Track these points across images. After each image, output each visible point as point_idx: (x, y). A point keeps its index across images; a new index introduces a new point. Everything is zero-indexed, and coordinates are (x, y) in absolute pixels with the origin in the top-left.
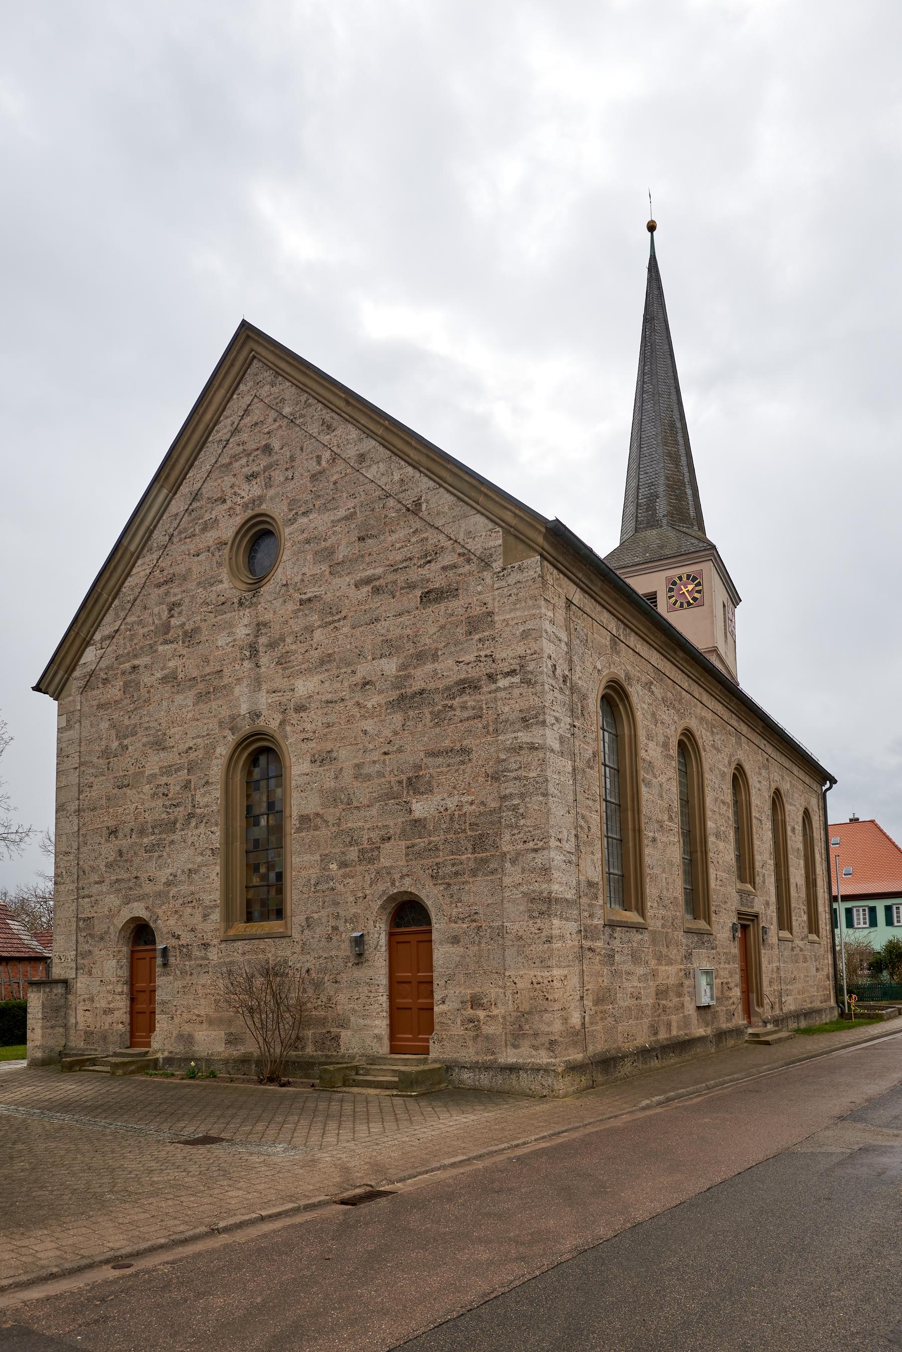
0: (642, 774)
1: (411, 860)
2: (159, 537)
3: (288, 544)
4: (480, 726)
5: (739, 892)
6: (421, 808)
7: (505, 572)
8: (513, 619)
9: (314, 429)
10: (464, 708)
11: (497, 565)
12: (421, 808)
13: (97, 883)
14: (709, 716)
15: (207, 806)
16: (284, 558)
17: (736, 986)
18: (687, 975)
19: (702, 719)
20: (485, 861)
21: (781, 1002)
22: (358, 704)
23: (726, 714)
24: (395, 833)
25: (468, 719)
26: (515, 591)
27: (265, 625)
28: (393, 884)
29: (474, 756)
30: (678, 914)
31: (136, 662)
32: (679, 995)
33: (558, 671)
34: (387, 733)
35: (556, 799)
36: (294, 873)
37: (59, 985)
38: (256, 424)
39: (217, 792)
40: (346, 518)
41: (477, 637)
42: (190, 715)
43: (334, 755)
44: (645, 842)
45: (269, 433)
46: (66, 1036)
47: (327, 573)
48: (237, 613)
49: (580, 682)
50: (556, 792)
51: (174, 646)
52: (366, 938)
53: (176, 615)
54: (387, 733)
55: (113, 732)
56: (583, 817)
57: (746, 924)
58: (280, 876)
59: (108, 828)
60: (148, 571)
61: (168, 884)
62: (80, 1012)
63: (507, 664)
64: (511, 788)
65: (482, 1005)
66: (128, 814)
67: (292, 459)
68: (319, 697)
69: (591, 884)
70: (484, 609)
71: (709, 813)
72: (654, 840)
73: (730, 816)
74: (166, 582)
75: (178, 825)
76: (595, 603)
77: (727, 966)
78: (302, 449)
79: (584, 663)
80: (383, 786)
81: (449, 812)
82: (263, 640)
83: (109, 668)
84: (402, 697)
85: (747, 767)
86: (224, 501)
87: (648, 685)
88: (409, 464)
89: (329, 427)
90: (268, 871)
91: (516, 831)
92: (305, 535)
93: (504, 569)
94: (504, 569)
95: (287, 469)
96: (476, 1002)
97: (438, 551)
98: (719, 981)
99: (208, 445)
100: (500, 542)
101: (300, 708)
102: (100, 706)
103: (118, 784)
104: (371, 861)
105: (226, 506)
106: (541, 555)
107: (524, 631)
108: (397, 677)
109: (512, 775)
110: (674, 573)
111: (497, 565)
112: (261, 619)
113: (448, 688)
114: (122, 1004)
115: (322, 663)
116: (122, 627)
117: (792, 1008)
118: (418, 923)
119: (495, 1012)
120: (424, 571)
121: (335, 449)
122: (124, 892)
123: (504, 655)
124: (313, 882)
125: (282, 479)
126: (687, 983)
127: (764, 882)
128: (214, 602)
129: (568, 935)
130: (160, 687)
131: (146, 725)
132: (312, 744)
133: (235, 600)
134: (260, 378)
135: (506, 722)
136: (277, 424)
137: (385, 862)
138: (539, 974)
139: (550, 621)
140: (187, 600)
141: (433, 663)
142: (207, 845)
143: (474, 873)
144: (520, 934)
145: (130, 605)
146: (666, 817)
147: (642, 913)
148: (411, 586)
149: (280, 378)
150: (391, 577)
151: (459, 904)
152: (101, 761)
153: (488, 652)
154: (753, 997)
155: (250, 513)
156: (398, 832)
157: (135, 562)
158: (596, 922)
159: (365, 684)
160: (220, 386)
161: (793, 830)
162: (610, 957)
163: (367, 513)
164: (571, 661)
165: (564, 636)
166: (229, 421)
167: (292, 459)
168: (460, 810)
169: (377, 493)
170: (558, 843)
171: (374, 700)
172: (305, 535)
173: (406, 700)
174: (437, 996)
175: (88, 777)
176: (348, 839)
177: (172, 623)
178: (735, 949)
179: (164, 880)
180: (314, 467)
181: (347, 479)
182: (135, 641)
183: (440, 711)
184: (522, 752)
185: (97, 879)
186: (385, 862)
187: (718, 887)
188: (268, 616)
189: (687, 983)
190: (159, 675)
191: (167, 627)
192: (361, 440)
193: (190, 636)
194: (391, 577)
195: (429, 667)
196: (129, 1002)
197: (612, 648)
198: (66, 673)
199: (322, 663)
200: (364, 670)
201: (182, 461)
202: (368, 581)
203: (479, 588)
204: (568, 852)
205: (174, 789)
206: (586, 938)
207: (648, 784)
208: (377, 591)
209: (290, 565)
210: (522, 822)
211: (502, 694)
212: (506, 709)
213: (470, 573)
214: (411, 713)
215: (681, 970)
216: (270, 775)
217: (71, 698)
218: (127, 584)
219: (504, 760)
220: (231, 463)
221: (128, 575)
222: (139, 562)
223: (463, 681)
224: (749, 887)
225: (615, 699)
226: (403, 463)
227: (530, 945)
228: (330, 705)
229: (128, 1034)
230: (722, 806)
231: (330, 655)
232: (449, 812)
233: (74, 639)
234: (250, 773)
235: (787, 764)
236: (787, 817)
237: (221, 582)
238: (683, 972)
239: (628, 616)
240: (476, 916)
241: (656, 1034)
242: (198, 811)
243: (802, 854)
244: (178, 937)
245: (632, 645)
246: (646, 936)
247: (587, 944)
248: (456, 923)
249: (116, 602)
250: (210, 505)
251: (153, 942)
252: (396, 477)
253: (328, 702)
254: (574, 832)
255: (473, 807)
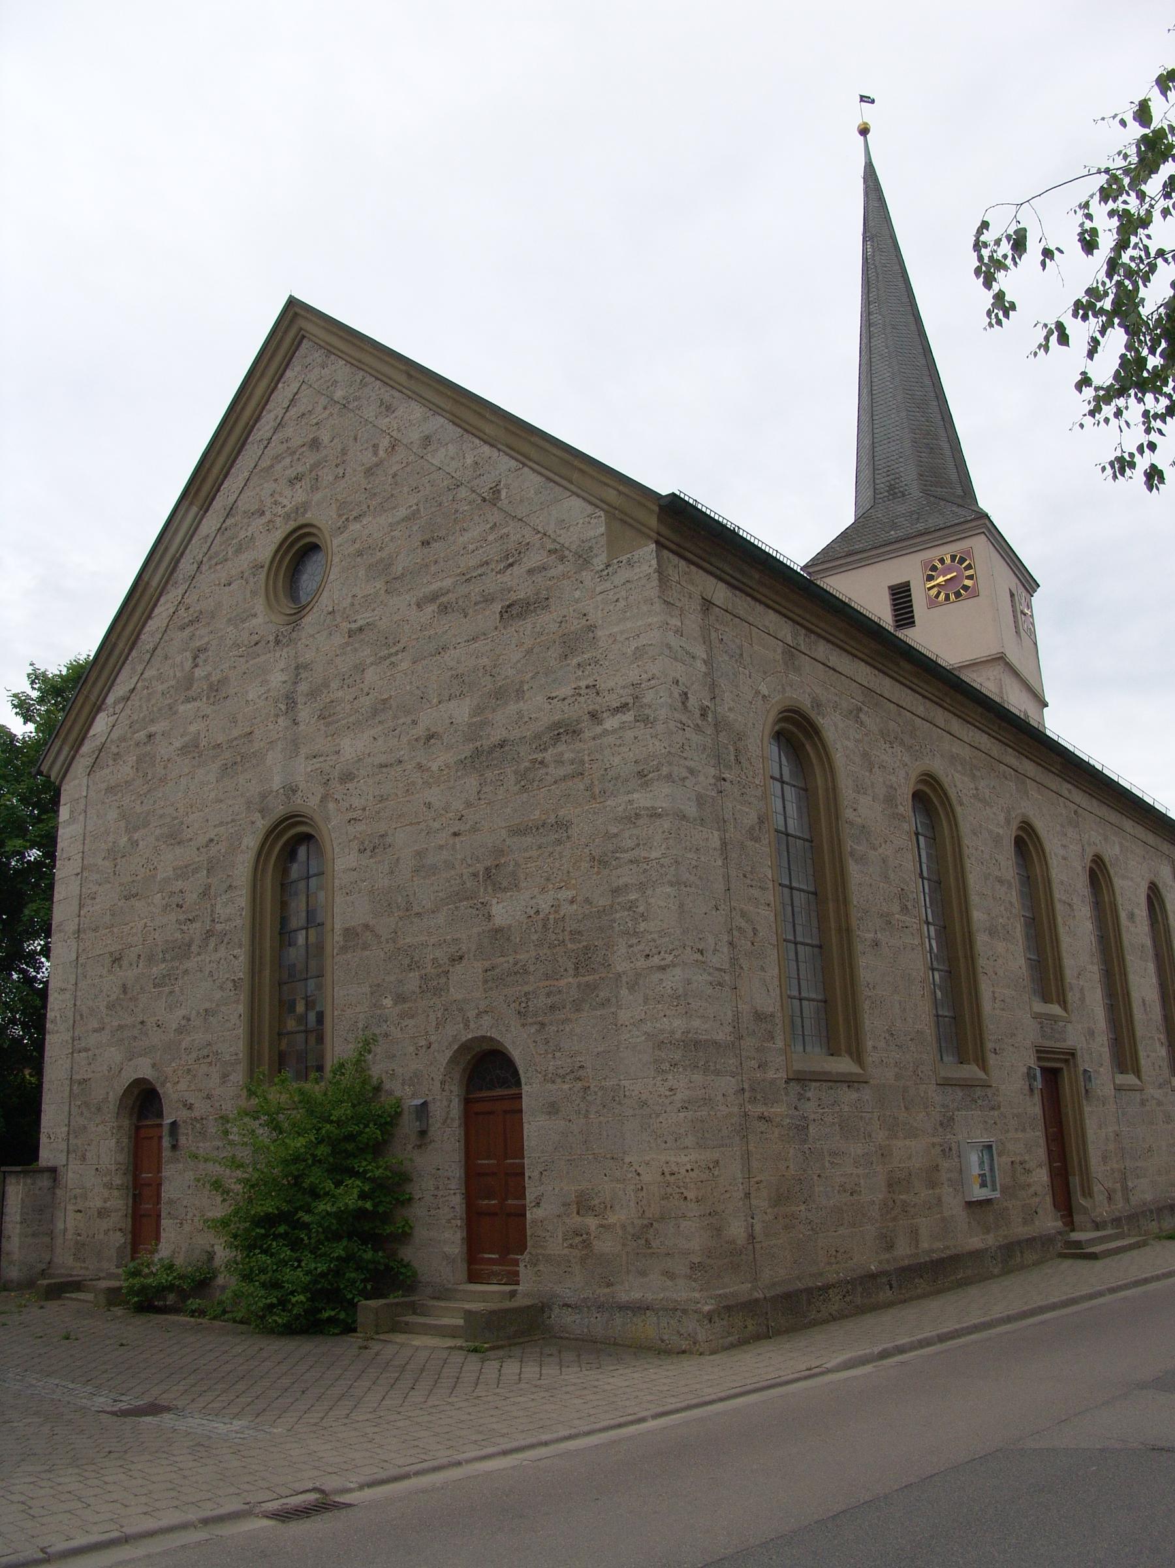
0: (849, 844)
1: (491, 989)
2: (186, 566)
3: (336, 560)
4: (582, 787)
5: (1036, 1016)
6: (504, 911)
7: (610, 569)
8: (622, 632)
9: (369, 412)
10: (560, 762)
11: (599, 562)
12: (504, 911)
13: (95, 1031)
14: (966, 752)
15: (229, 920)
16: (332, 577)
17: (1040, 1166)
18: (946, 1152)
19: (953, 759)
20: (592, 988)
21: (1125, 1189)
22: (420, 766)
23: (995, 749)
24: (469, 950)
25: (564, 778)
26: (623, 593)
27: (306, 667)
28: (467, 1026)
29: (574, 831)
30: (925, 1056)
31: (153, 729)
32: (932, 1184)
33: (692, 702)
34: (457, 805)
35: (693, 889)
36: (336, 1013)
37: (46, 1175)
38: (304, 414)
39: (242, 899)
40: (407, 519)
41: (575, 661)
42: (213, 795)
43: (389, 840)
44: (859, 947)
45: (317, 424)
46: (51, 1248)
47: (382, 592)
48: (272, 655)
49: (732, 716)
50: (692, 878)
51: (196, 704)
52: (431, 1107)
53: (201, 664)
54: (457, 805)
55: (123, 824)
56: (743, 914)
57: (1054, 1076)
58: (320, 1018)
59: (111, 954)
60: (172, 610)
61: (180, 1031)
62: (71, 1215)
63: (615, 696)
64: (626, 876)
65: (592, 1209)
66: (136, 934)
67: (344, 452)
68: (370, 760)
69: (759, 1017)
70: (584, 622)
71: (974, 899)
72: (876, 944)
73: (1014, 900)
74: (191, 622)
75: (194, 948)
76: (752, 603)
77: (1020, 1135)
78: (356, 439)
79: (737, 686)
80: (453, 882)
81: (541, 916)
82: (303, 687)
83: (123, 739)
84: (478, 752)
85: (1039, 825)
86: (263, 513)
87: (855, 714)
88: (485, 442)
89: (388, 408)
90: (307, 1010)
91: (634, 941)
92: (357, 546)
93: (608, 566)
94: (608, 566)
95: (337, 466)
96: (583, 1204)
97: (524, 548)
98: (1005, 1160)
99: (247, 447)
100: (603, 529)
101: (347, 777)
102: (110, 790)
103: (125, 893)
104: (438, 991)
105: (264, 520)
106: (657, 542)
107: (637, 648)
108: (470, 725)
109: (627, 856)
110: (933, 554)
111: (599, 562)
112: (301, 660)
113: (537, 736)
114: (119, 1203)
115: (375, 712)
116: (139, 684)
117: (1148, 1197)
118: (504, 1083)
119: (612, 1219)
120: (506, 578)
121: (394, 434)
122: (126, 1043)
123: (611, 684)
124: (360, 1025)
125: (331, 478)
126: (945, 1164)
127: (1082, 999)
128: (246, 642)
129: (720, 1097)
130: (178, 759)
131: (161, 812)
132: (361, 827)
133: (271, 638)
134: (309, 360)
135: (616, 779)
136: (327, 412)
137: (456, 994)
138: (673, 1159)
139: (676, 632)
140: (214, 643)
141: (517, 702)
142: (227, 976)
143: (577, 1007)
144: (644, 1097)
145: (148, 656)
146: (896, 908)
147: (858, 1056)
148: (488, 599)
149: (333, 357)
150: (463, 590)
151: (558, 1054)
152: (107, 863)
153: (590, 682)
154: (1075, 1181)
155: (292, 525)
156: (474, 948)
157: (158, 600)
158: (771, 1074)
159: (431, 737)
160: (262, 375)
161: (1131, 916)
162: (801, 1129)
163: (433, 509)
164: (713, 686)
165: (700, 652)
166: (272, 416)
167: (344, 452)
168: (556, 912)
169: (446, 483)
170: (698, 956)
171: (441, 758)
172: (357, 546)
173: (483, 757)
174: (531, 1194)
175: (91, 885)
176: (407, 961)
177: (196, 674)
178: (1034, 1108)
179: (174, 1026)
180: (368, 458)
181: (408, 469)
182: (153, 701)
183: (527, 769)
184: (640, 822)
185: (96, 1026)
186: (456, 994)
187: (997, 1012)
188: (308, 656)
189: (945, 1164)
190: (178, 744)
191: (189, 681)
192: (425, 419)
193: (216, 690)
194: (463, 590)
195: (512, 708)
196: (131, 1201)
197: (786, 663)
198: (71, 749)
199: (375, 712)
200: (428, 719)
201: (215, 471)
202: (433, 597)
203: (577, 594)
204: (717, 969)
205: (192, 897)
206: (753, 1100)
207: (862, 859)
208: (444, 609)
209: (336, 584)
210: (642, 926)
211: (611, 739)
212: (617, 760)
213: (565, 576)
214: (489, 775)
215: (934, 1145)
216: (311, 872)
217: (77, 782)
218: (147, 629)
219: (616, 835)
220: (272, 466)
221: (149, 617)
222: (162, 600)
223: (557, 725)
224: (1056, 1009)
225: (797, 734)
226: (477, 441)
227: (658, 1116)
228: (384, 770)
229: (129, 1247)
230: (998, 886)
231: (384, 701)
232: (541, 916)
233: (84, 703)
234: (285, 872)
235: (1113, 817)
236: (1119, 898)
237: (255, 615)
238: (938, 1149)
239: (808, 617)
240: (581, 1073)
241: (890, 1247)
242: (219, 927)
243: (1150, 952)
244: (190, 1107)
245: (820, 656)
246: (866, 1094)
247: (757, 1109)
248: (553, 1082)
249: (134, 653)
250: (246, 520)
251: (160, 1115)
252: (469, 461)
253: (381, 766)
254: (725, 938)
255: (575, 907)
